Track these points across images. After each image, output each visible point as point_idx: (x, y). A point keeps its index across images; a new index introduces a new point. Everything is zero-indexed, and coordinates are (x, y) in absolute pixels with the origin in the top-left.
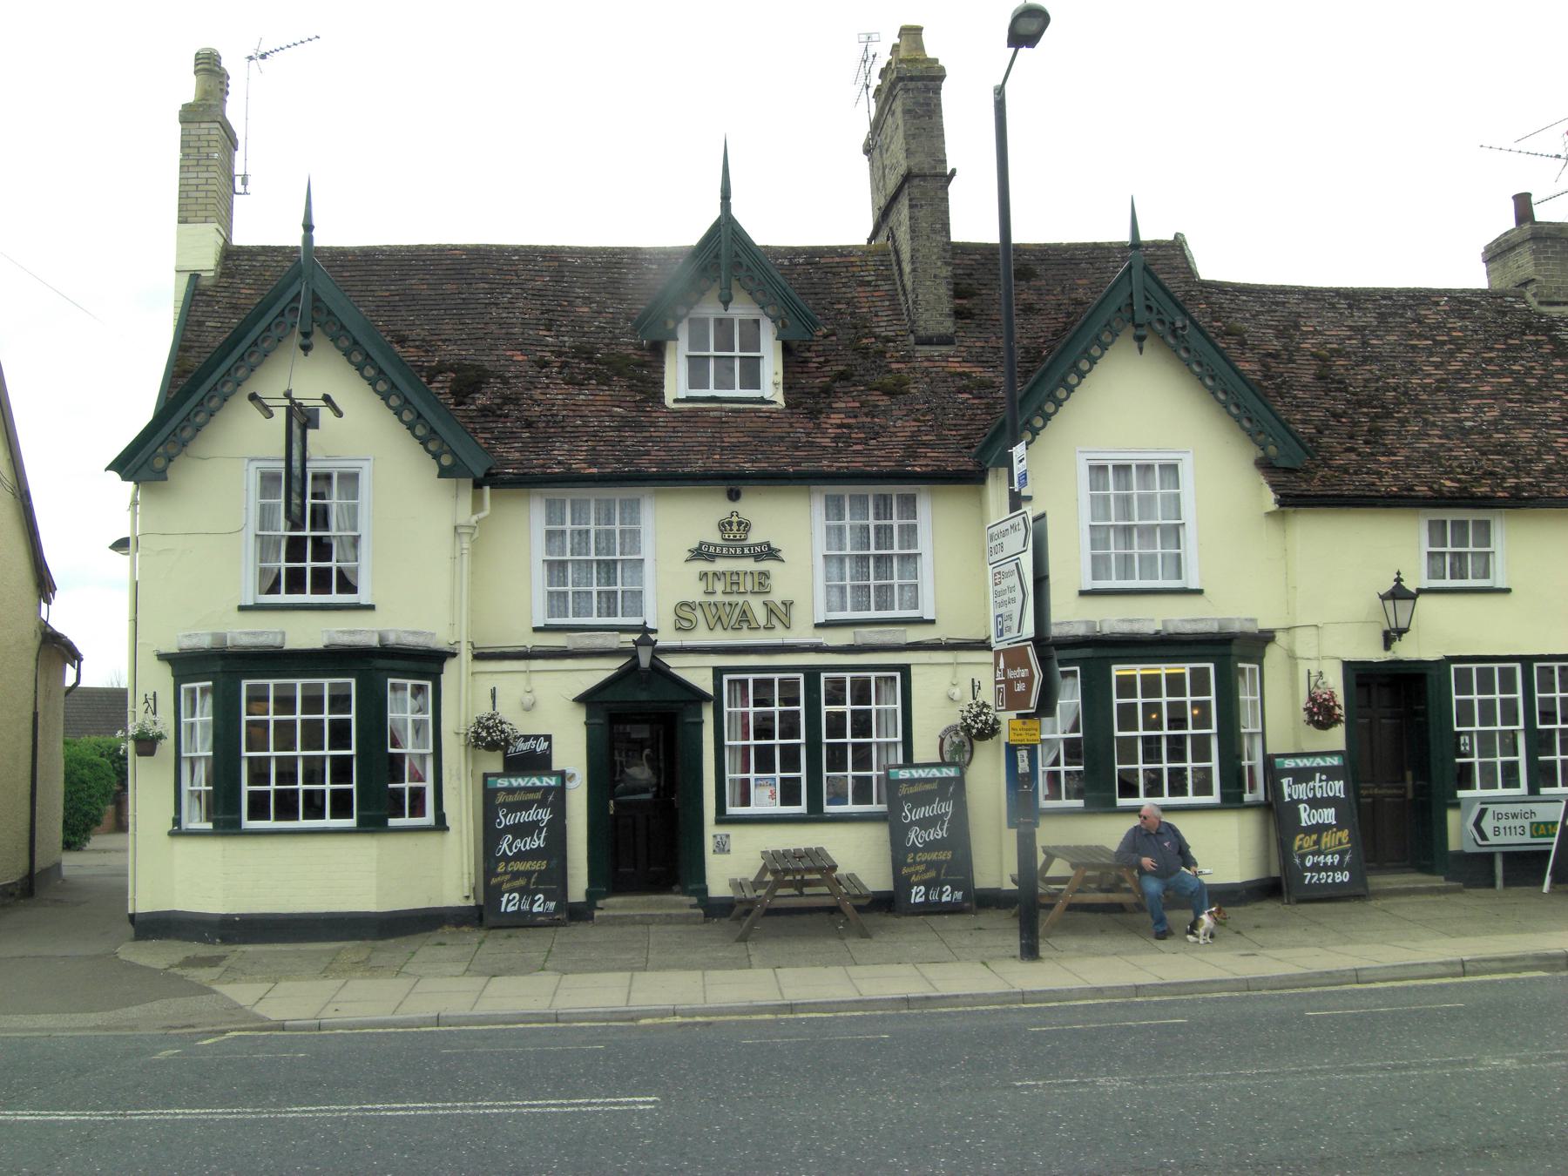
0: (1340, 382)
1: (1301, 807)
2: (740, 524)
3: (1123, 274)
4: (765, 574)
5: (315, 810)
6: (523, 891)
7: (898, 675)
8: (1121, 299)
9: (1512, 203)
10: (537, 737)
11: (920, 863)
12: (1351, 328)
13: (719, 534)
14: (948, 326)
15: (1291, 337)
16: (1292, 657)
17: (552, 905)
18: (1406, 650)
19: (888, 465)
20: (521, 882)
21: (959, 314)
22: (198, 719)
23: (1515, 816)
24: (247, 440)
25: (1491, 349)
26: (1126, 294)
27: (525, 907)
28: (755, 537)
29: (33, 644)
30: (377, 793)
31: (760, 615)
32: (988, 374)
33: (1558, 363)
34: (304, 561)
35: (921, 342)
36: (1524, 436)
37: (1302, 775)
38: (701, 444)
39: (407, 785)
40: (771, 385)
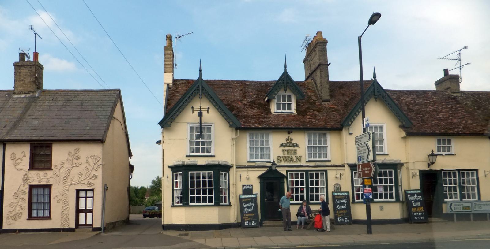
0: (412, 109)
1: (413, 202)
2: (290, 139)
3: (373, 84)
4: (296, 150)
5: (204, 200)
6: (342, 217)
7: (325, 172)
8: (372, 90)
9: (443, 71)
10: (249, 185)
11: (247, 216)
12: (411, 99)
13: (286, 141)
14: (328, 98)
15: (399, 100)
16: (408, 169)
17: (349, 220)
18: (433, 168)
19: (321, 126)
20: (341, 215)
21: (331, 95)
22: (178, 181)
23: (459, 205)
24: (189, 118)
25: (443, 103)
26: (373, 88)
27: (343, 221)
28: (293, 142)
29: (128, 167)
30: (218, 199)
31: (295, 159)
32: (338, 108)
33: (458, 105)
34: (199, 146)
35: (323, 101)
36: (455, 121)
37: (412, 195)
38: (281, 122)
39: (223, 195)
40: (294, 109)
